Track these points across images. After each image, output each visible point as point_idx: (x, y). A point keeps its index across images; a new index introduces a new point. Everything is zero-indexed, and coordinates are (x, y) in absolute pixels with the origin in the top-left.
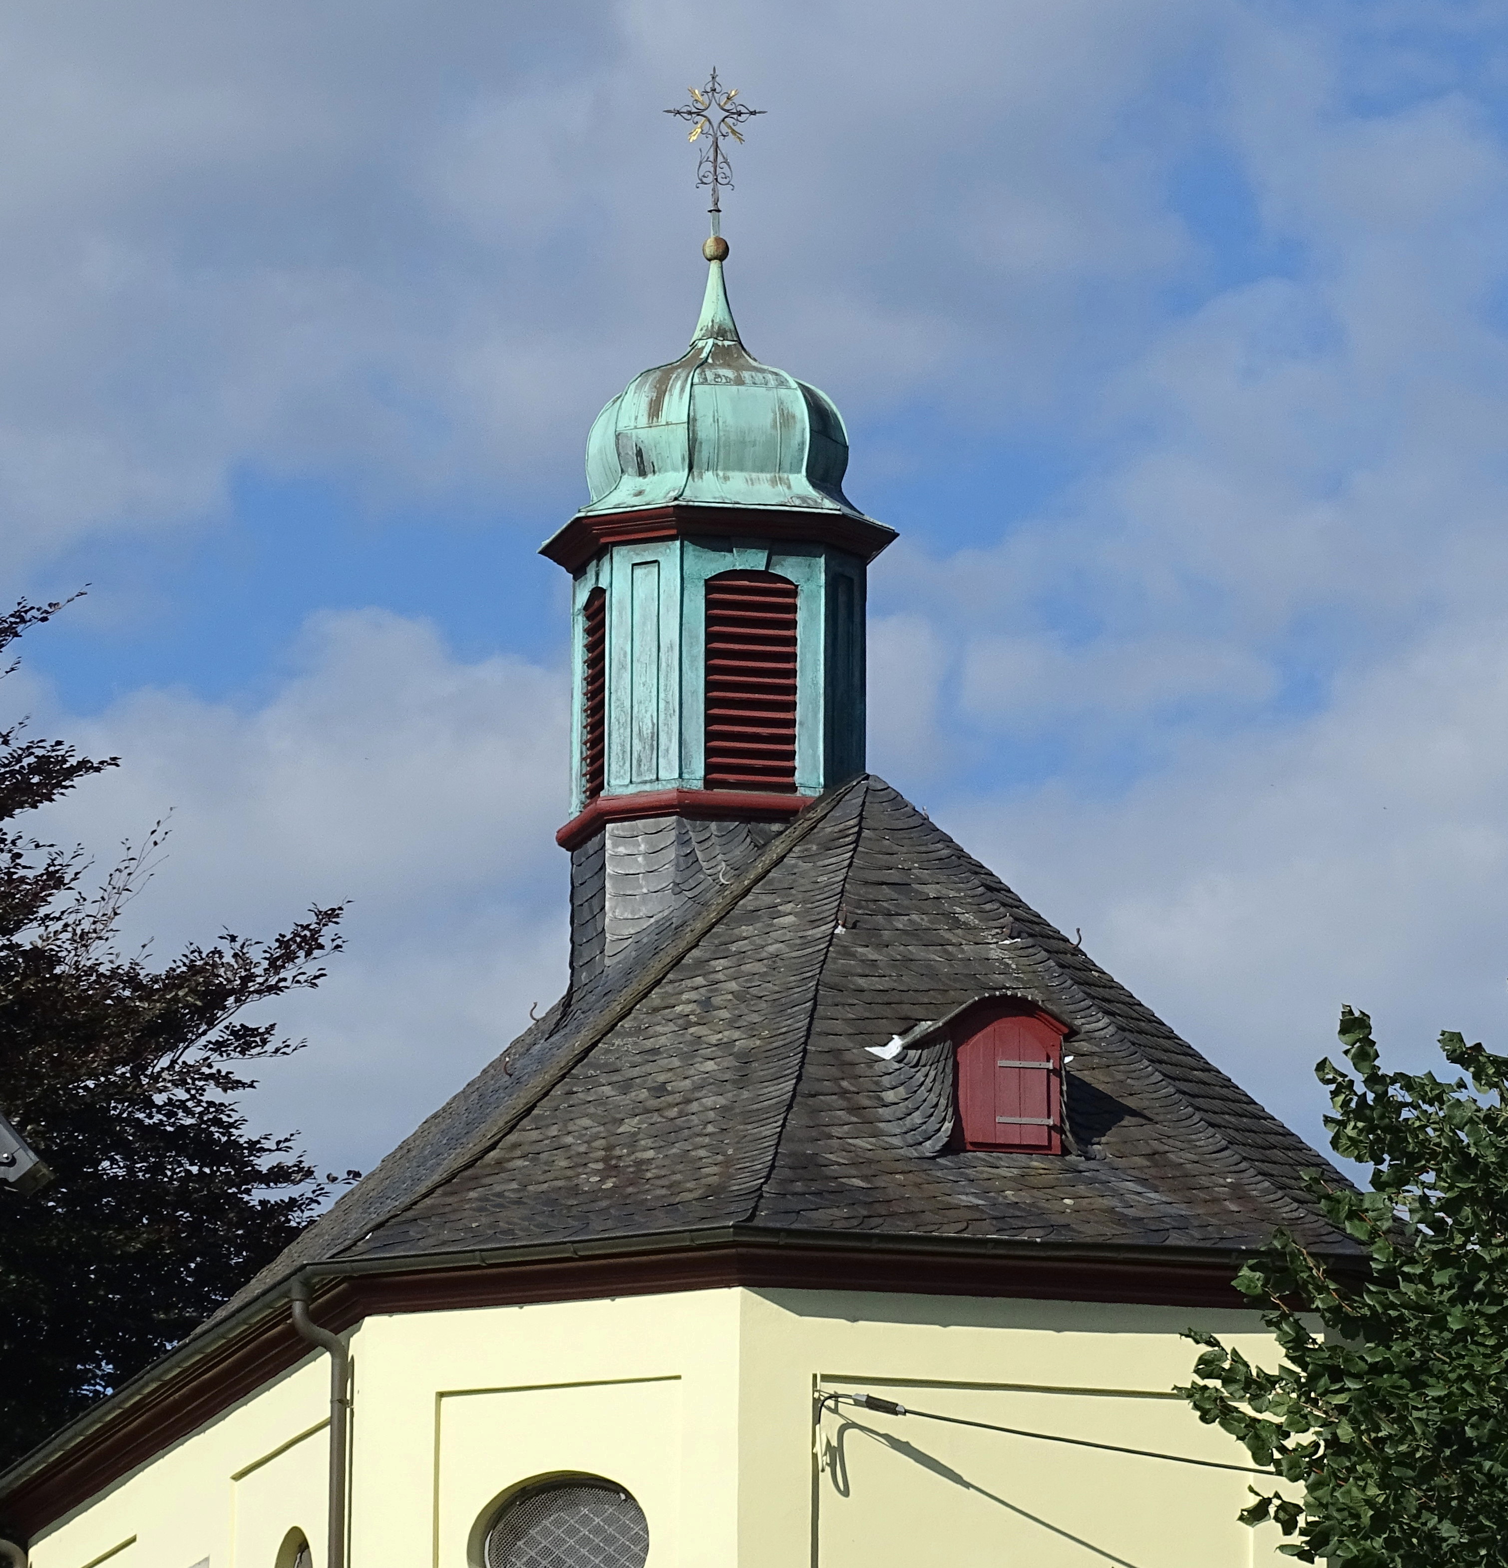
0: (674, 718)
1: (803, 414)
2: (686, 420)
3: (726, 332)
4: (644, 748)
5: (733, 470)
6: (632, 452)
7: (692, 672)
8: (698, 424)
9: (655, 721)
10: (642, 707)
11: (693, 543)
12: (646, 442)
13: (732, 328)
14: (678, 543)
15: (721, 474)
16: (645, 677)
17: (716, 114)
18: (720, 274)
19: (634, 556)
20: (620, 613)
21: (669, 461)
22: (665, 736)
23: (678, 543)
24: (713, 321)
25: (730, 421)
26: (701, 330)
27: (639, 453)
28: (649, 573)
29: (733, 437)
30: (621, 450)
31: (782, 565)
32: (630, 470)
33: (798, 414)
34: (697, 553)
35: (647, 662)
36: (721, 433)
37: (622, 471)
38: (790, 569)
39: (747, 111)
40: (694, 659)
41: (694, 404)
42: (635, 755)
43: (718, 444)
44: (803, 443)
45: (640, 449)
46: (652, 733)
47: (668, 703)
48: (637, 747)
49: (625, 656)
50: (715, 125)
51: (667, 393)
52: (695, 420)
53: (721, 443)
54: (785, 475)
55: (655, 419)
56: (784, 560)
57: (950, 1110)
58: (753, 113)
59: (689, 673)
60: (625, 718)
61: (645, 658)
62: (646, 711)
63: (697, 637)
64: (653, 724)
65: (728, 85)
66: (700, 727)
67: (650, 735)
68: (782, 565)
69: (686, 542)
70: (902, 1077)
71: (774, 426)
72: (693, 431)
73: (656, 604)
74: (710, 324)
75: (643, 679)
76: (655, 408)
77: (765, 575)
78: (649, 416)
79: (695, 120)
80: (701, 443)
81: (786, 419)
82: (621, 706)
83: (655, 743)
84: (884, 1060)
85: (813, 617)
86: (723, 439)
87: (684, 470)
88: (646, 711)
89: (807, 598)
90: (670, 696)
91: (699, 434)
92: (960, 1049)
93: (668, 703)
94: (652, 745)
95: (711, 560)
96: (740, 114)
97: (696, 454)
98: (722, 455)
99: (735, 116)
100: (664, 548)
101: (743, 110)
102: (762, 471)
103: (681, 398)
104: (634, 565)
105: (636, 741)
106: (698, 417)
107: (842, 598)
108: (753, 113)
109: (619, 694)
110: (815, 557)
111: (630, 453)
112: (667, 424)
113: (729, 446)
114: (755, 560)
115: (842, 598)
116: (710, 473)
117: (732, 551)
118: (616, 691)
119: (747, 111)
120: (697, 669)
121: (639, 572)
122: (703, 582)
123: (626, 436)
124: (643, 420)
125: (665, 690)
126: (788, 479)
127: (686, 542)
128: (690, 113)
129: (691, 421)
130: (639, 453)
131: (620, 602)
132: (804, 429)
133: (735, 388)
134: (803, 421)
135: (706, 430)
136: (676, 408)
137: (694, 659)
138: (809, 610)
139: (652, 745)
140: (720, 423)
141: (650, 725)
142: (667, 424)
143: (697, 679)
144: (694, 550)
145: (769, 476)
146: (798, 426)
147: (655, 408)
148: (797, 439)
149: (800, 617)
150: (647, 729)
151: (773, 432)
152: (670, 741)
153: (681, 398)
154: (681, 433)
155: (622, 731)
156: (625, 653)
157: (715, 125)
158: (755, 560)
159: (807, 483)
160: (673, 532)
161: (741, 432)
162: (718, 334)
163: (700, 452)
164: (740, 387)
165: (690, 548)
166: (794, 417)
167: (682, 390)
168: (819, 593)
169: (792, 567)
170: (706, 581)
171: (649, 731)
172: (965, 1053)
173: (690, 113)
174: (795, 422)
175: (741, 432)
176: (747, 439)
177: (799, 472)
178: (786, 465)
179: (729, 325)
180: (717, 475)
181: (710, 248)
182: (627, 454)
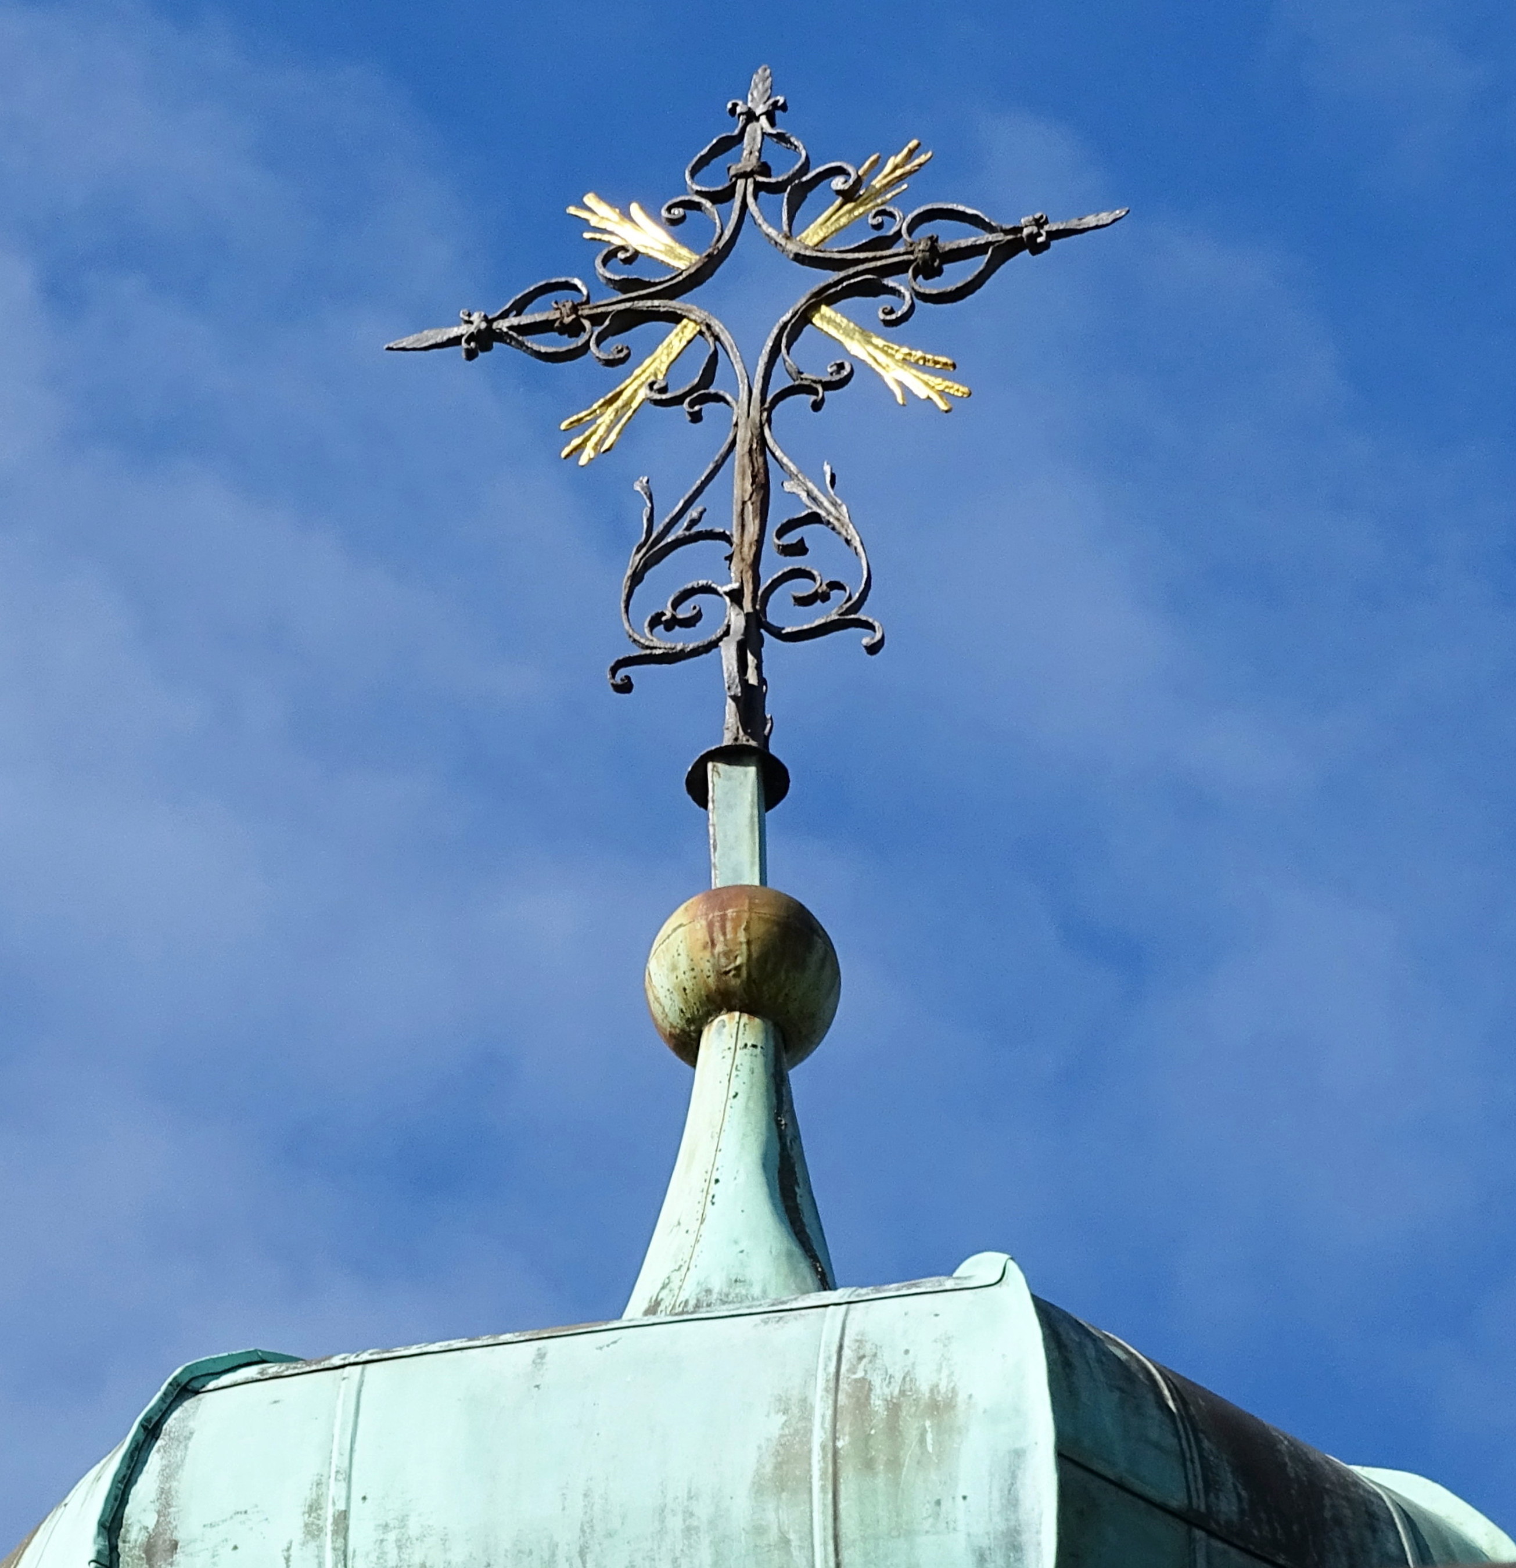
41: (168, 1474)
71: (784, 1474)
101: (955, 237)
106: (187, 1528)
151: (777, 1515)
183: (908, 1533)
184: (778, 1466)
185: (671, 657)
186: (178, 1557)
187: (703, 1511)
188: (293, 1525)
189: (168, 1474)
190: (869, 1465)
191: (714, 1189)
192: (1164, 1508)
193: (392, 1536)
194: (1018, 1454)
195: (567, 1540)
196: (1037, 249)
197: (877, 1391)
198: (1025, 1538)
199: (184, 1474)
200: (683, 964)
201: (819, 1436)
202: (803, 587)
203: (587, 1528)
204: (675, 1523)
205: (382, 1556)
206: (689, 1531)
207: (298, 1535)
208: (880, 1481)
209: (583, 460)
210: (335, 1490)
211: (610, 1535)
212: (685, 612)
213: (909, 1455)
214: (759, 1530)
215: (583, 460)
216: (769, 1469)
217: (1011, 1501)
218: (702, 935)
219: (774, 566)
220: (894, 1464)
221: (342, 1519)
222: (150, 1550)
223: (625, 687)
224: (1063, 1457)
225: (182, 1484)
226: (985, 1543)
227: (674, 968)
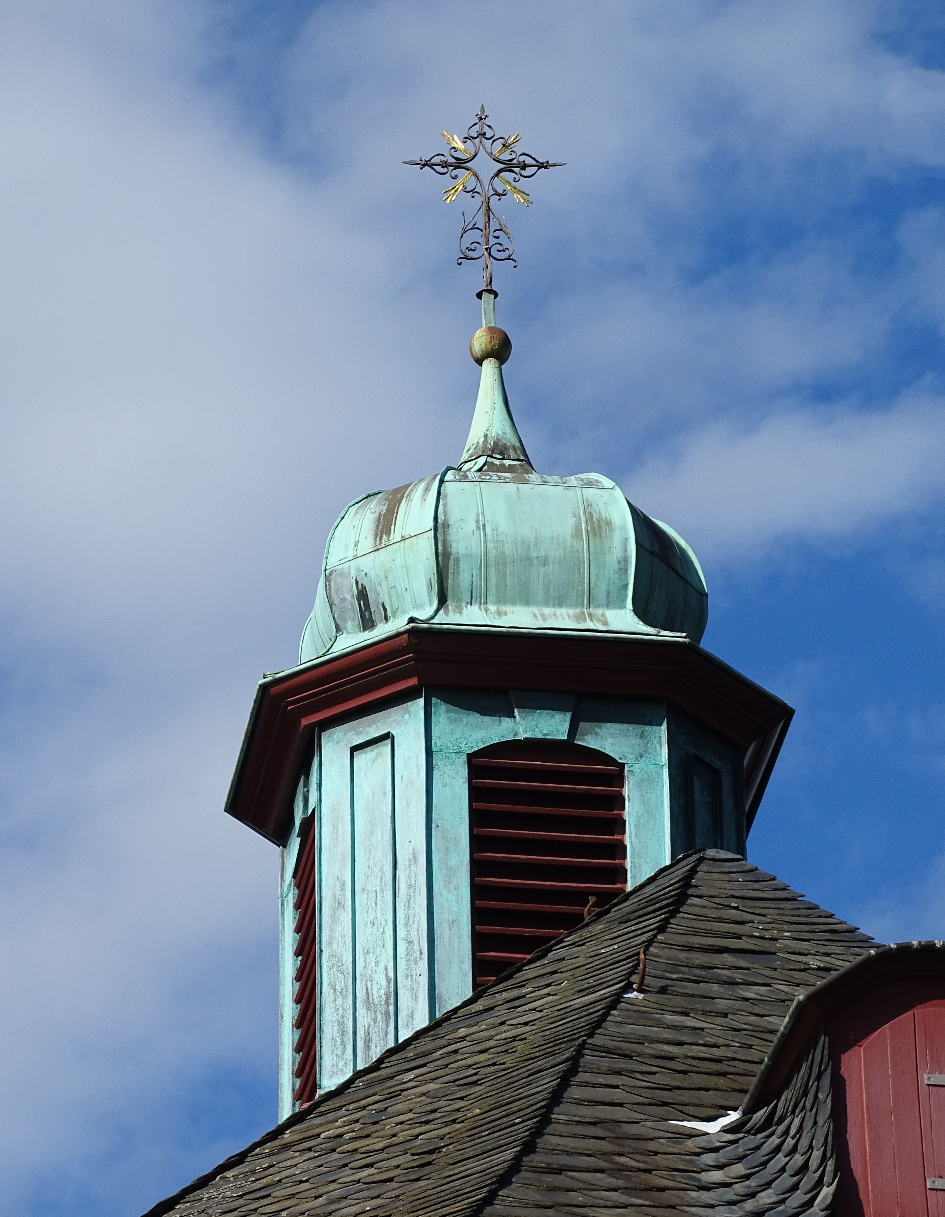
0: (420, 963)
1: (624, 518)
2: (431, 524)
3: (505, 447)
4: (375, 1020)
5: (513, 603)
6: (350, 596)
7: (449, 891)
8: (452, 531)
9: (391, 974)
10: (371, 959)
11: (446, 700)
12: (372, 574)
13: (517, 444)
14: (421, 702)
15: (492, 608)
16: (374, 911)
17: (485, 166)
18: (497, 377)
19: (355, 737)
20: (335, 827)
21: (408, 596)
22: (408, 994)
23: (421, 702)
24: (486, 436)
25: (504, 527)
26: (469, 450)
27: (362, 595)
28: (379, 755)
29: (508, 550)
30: (334, 595)
31: (596, 734)
32: (350, 624)
33: (616, 520)
34: (453, 715)
35: (378, 888)
36: (490, 545)
37: (338, 629)
38: (608, 739)
39: (534, 162)
40: (451, 873)
41: (445, 506)
42: (361, 1034)
43: (486, 562)
44: (626, 560)
45: (364, 588)
46: (387, 995)
47: (410, 942)
48: (364, 1018)
49: (343, 889)
50: (486, 180)
51: (404, 501)
52: (446, 525)
53: (491, 561)
54: (599, 611)
55: (385, 537)
56: (600, 727)
57: (830, 1165)
58: (542, 166)
59: (444, 892)
60: (344, 982)
61: (374, 884)
62: (377, 963)
63: (457, 840)
64: (388, 981)
65: (501, 125)
66: (465, 975)
67: (384, 998)
68: (596, 734)
69: (434, 700)
70: (741, 1150)
71: (577, 534)
72: (445, 541)
73: (392, 801)
74: (482, 439)
75: (372, 916)
76: (384, 526)
77: (566, 749)
78: (376, 535)
79: (453, 174)
80: (457, 560)
81: (597, 527)
82: (338, 966)
83: (392, 1008)
84: (709, 1134)
85: (651, 812)
86: (493, 553)
87: (431, 604)
88: (377, 963)
89: (639, 784)
90: (414, 933)
91: (454, 545)
92: (845, 1057)
93: (410, 942)
94: (387, 1013)
95: (478, 727)
96: (524, 166)
97: (450, 577)
98: (493, 579)
99: (517, 170)
100: (402, 712)
101: (529, 161)
102: (560, 605)
103: (424, 499)
104: (354, 749)
105: (361, 1011)
106: (451, 522)
107: (700, 796)
108: (542, 166)
109: (335, 946)
110: (650, 723)
111: (349, 597)
112: (403, 539)
113: (504, 564)
114: (552, 725)
115: (700, 796)
116: (475, 607)
117: (512, 716)
118: (330, 943)
119: (534, 162)
120: (457, 888)
121: (361, 758)
122: (464, 758)
123: (342, 574)
124: (367, 543)
125: (406, 925)
126: (603, 615)
127: (434, 700)
128: (445, 165)
129: (439, 528)
130: (362, 595)
131: (333, 809)
132: (626, 540)
133: (513, 486)
134: (624, 528)
135: (464, 540)
136: (416, 515)
137: (451, 873)
138: (645, 802)
139: (387, 1013)
140: (489, 531)
141: (384, 983)
142: (403, 539)
143: (457, 902)
144: (447, 711)
145: (571, 612)
146: (617, 536)
147: (384, 526)
148: (616, 553)
149: (630, 813)
150: (379, 987)
151: (576, 544)
152: (416, 1000)
153: (424, 499)
154: (425, 547)
155: (339, 1001)
156: (343, 884)
157: (486, 180)
158: (552, 725)
159: (636, 619)
160: (413, 682)
161: (523, 542)
162: (493, 451)
163: (456, 573)
164: (520, 486)
165: (443, 714)
166: (609, 523)
167: (427, 489)
168: (660, 775)
169: (612, 735)
170: (470, 757)
171: (382, 992)
172: (856, 1064)
173: (445, 165)
174: (611, 530)
175: (523, 542)
176: (534, 554)
177: (623, 606)
178: (600, 592)
179: (510, 438)
180: (486, 610)
181: (480, 341)
182: (344, 599)
183: (604, 553)
184: (576, 532)
185: (471, 259)
186: (450, 528)
187: (561, 539)
188: (473, 525)
189: (445, 506)
190: (595, 535)
191: (495, 405)
192: (648, 550)
193: (495, 532)
194: (627, 539)
195: (532, 540)
196: (546, 168)
197: (594, 516)
198: (629, 559)
199: (448, 506)
200: (484, 345)
201: (583, 526)
202: (500, 248)
203: (536, 539)
204: (555, 541)
205: (493, 537)
206: (558, 544)
207: (475, 528)
208: (598, 540)
209: (448, 202)
210: (481, 518)
211: (541, 541)
212: (473, 247)
213: (603, 535)
214: (573, 547)
215: (448, 202)
216: (574, 532)
217: (625, 551)
218: (489, 340)
219: (492, 241)
220: (601, 536)
221: (484, 525)
222: (443, 525)
223: (460, 264)
224: (637, 542)
225: (448, 509)
226: (620, 559)
227: (481, 345)
